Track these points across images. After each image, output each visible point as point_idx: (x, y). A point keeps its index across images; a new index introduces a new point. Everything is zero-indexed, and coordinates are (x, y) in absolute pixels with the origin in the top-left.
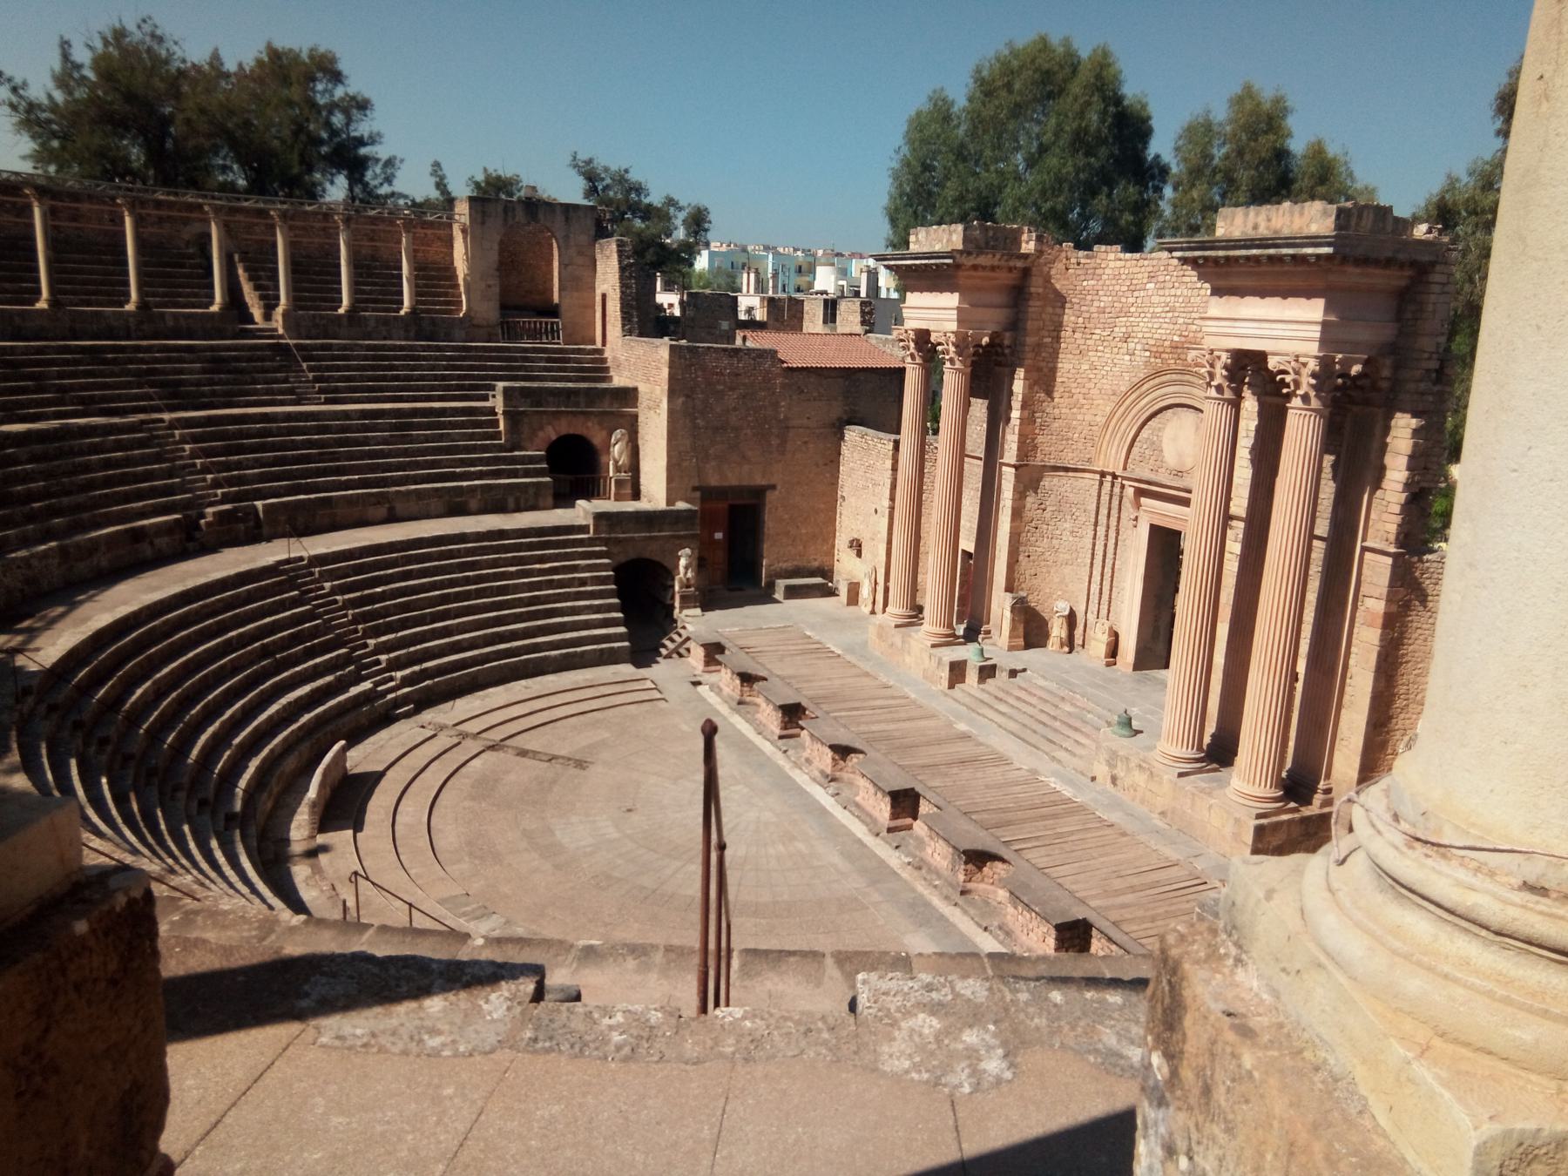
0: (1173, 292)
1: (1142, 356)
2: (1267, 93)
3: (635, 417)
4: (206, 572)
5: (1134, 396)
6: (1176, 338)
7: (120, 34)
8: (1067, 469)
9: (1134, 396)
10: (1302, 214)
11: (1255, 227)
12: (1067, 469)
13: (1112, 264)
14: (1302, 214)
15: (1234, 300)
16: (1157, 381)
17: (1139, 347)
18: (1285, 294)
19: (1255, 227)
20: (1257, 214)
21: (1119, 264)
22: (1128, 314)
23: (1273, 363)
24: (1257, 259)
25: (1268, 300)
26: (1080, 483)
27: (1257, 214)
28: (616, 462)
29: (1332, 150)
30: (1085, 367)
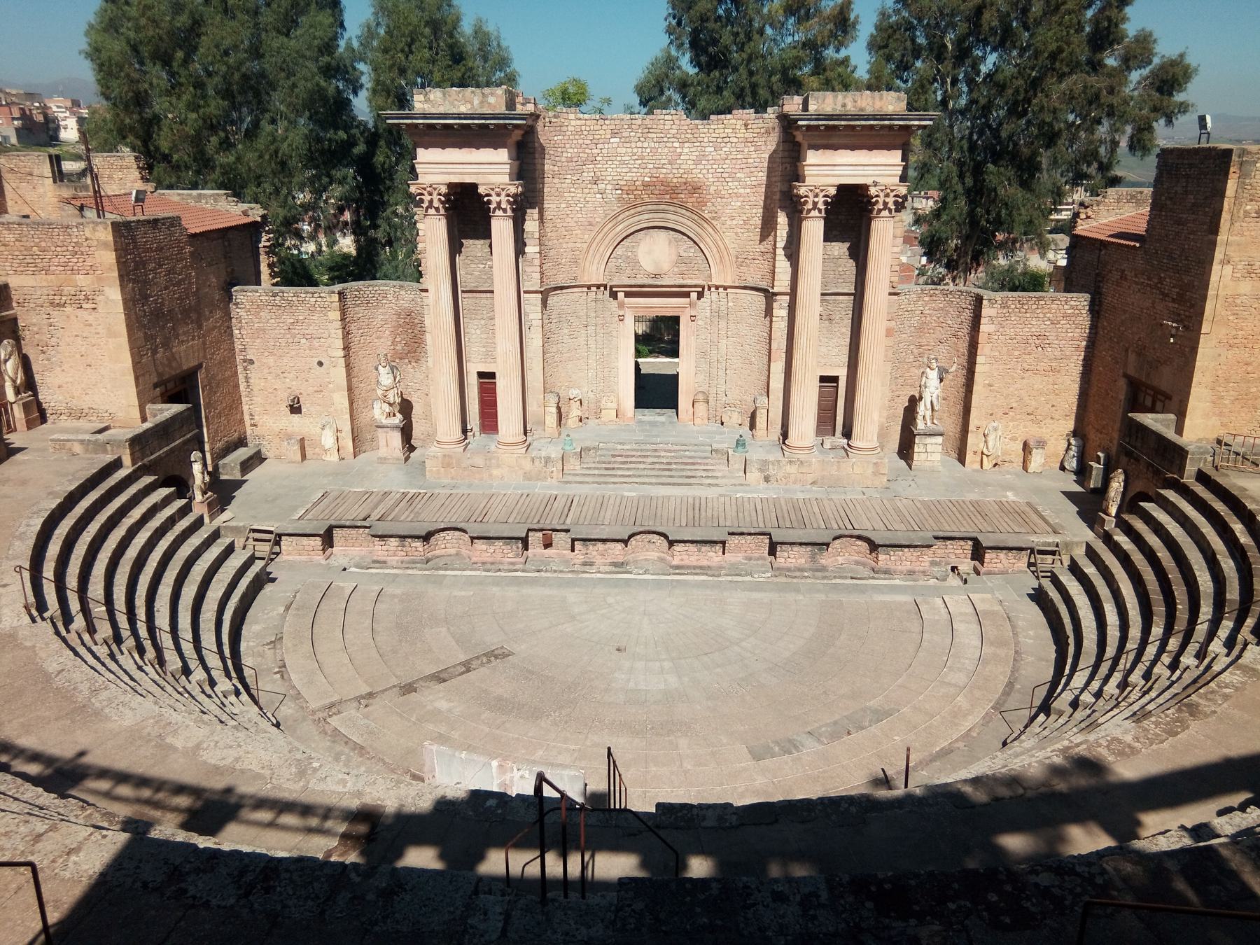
0: (639, 144)
1: (612, 195)
2: (1191, 60)
3: (15, 320)
4: (1161, 421)
5: (610, 225)
6: (647, 179)
7: (1151, 34)
8: (562, 288)
9: (610, 225)
10: (881, 99)
11: (844, 105)
12: (562, 288)
13: (573, 123)
14: (881, 99)
15: (829, 152)
16: (633, 211)
17: (609, 187)
18: (853, 148)
19: (844, 105)
20: (845, 97)
21: (579, 122)
22: (594, 162)
23: (481, 190)
24: (872, 127)
25: (857, 152)
26: (572, 296)
27: (845, 97)
28: (14, 381)
29: (490, 28)
30: (563, 205)
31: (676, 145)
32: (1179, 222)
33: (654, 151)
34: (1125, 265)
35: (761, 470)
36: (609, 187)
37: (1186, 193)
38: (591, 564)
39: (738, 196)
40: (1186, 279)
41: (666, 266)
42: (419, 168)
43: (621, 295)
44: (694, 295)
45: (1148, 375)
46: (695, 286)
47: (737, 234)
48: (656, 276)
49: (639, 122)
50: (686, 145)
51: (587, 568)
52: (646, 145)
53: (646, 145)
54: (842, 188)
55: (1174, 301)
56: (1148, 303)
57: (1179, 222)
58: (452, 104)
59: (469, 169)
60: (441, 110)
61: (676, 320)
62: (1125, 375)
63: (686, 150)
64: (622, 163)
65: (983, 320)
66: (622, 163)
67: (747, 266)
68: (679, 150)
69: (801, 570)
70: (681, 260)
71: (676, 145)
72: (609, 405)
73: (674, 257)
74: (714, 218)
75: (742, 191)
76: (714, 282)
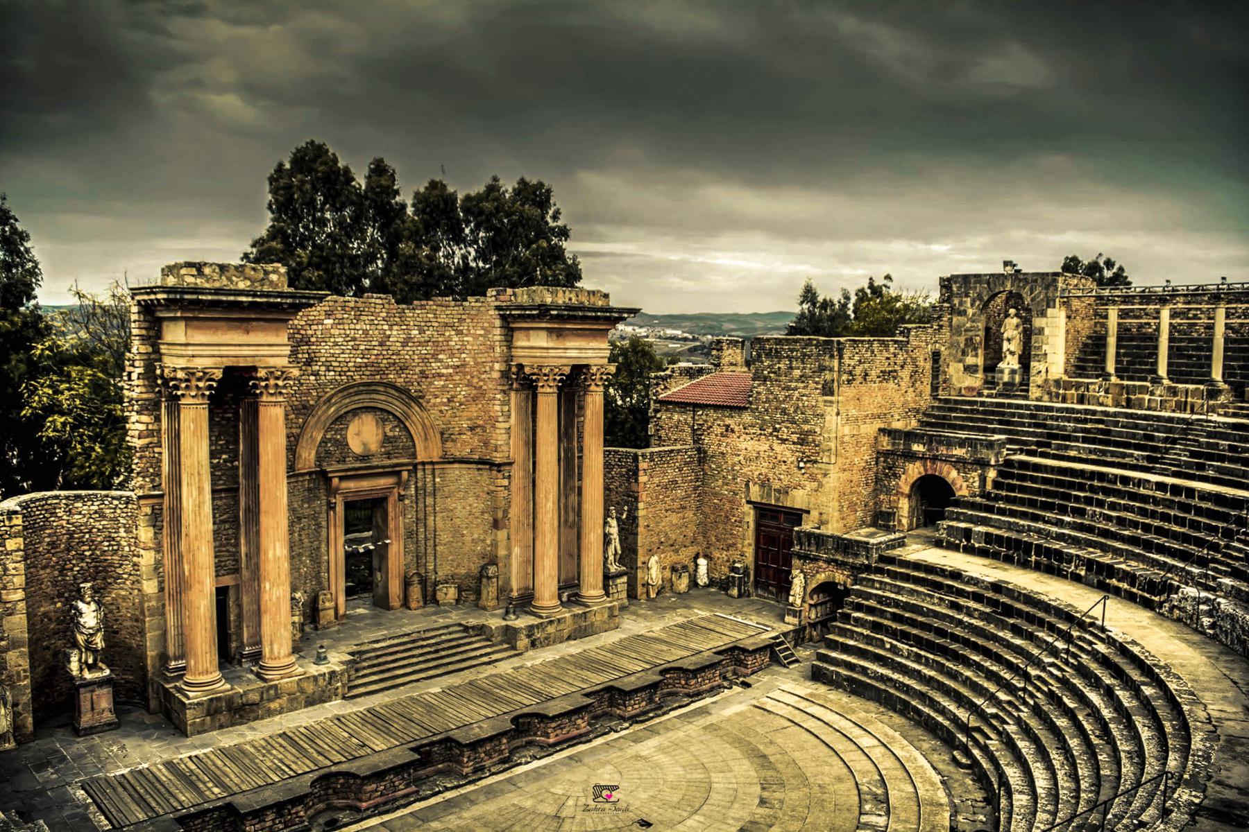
0: (352, 326)
6: (359, 360)
31: (386, 327)
32: (788, 388)
33: (366, 332)
34: (728, 421)
35: (529, 636)
36: (323, 368)
37: (791, 368)
38: (482, 769)
39: (440, 375)
40: (806, 427)
41: (374, 447)
42: (163, 349)
43: (336, 481)
44: (405, 475)
45: (777, 500)
46: (407, 465)
47: (441, 411)
48: (364, 457)
49: (352, 304)
50: (395, 328)
51: (479, 774)
52: (358, 327)
53: (358, 327)
54: (228, 371)
55: (794, 443)
56: (766, 447)
57: (788, 388)
58: (229, 279)
59: (246, 351)
60: (217, 285)
61: (384, 500)
62: (749, 502)
63: (395, 333)
64: (336, 344)
65: (641, 473)
66: (336, 344)
67: (453, 441)
68: (388, 333)
69: (644, 713)
70: (387, 439)
71: (386, 327)
72: (327, 604)
73: (381, 437)
74: (421, 397)
75: (444, 371)
76: (419, 459)
